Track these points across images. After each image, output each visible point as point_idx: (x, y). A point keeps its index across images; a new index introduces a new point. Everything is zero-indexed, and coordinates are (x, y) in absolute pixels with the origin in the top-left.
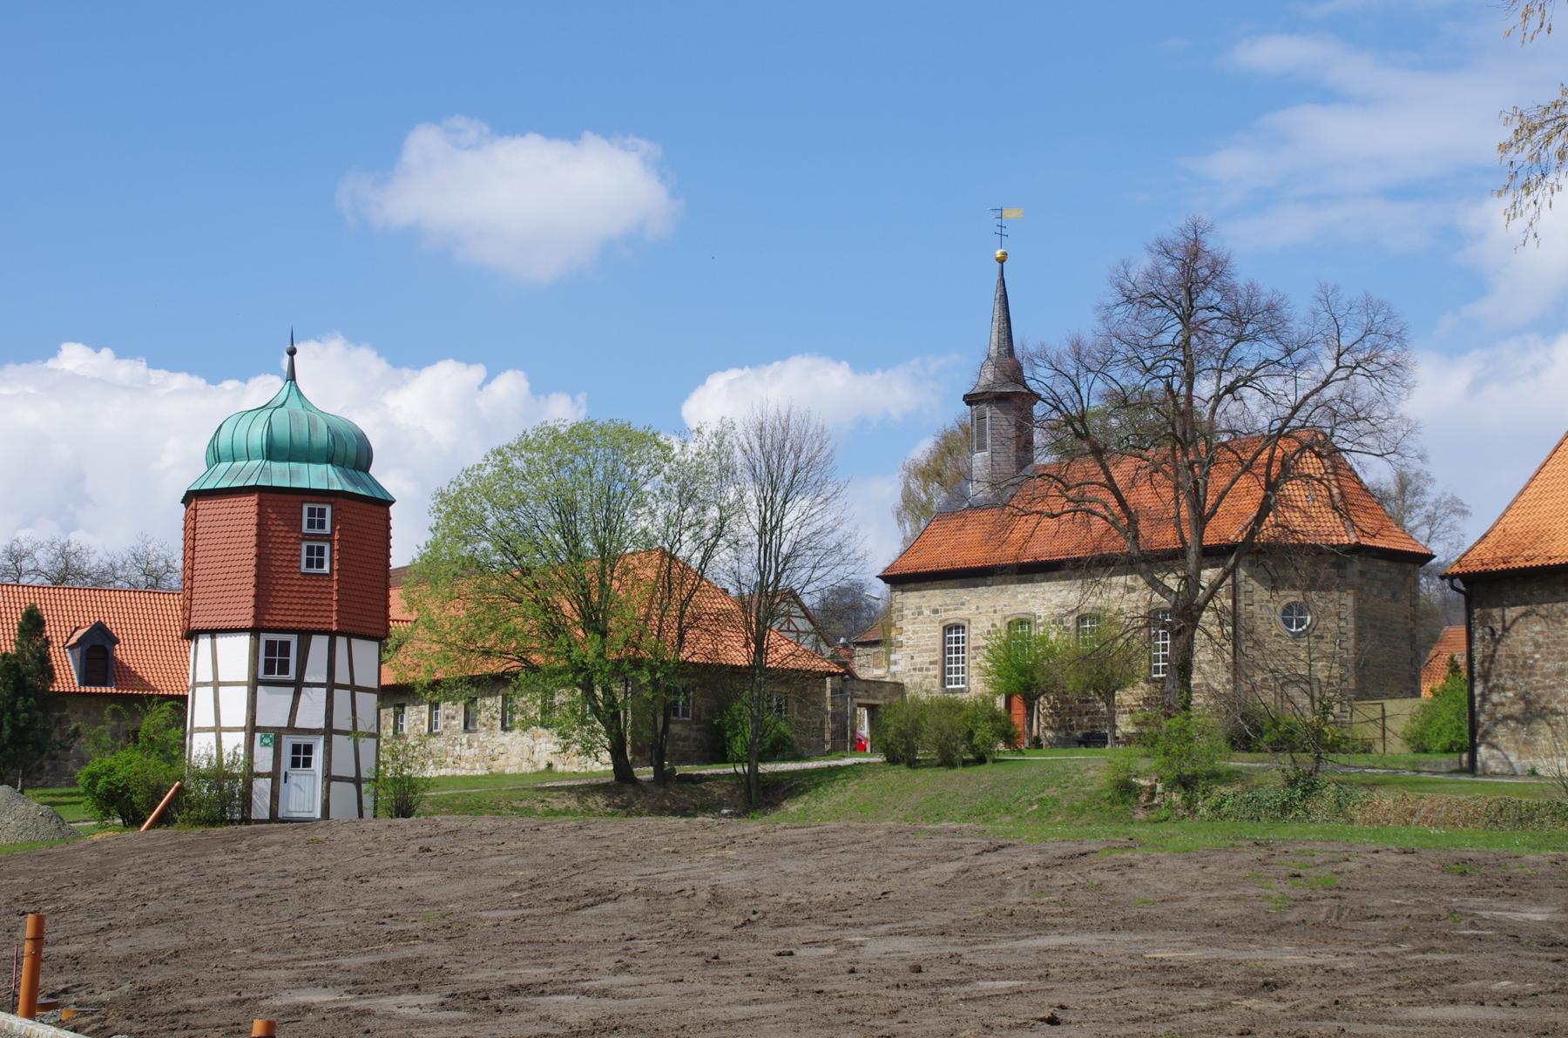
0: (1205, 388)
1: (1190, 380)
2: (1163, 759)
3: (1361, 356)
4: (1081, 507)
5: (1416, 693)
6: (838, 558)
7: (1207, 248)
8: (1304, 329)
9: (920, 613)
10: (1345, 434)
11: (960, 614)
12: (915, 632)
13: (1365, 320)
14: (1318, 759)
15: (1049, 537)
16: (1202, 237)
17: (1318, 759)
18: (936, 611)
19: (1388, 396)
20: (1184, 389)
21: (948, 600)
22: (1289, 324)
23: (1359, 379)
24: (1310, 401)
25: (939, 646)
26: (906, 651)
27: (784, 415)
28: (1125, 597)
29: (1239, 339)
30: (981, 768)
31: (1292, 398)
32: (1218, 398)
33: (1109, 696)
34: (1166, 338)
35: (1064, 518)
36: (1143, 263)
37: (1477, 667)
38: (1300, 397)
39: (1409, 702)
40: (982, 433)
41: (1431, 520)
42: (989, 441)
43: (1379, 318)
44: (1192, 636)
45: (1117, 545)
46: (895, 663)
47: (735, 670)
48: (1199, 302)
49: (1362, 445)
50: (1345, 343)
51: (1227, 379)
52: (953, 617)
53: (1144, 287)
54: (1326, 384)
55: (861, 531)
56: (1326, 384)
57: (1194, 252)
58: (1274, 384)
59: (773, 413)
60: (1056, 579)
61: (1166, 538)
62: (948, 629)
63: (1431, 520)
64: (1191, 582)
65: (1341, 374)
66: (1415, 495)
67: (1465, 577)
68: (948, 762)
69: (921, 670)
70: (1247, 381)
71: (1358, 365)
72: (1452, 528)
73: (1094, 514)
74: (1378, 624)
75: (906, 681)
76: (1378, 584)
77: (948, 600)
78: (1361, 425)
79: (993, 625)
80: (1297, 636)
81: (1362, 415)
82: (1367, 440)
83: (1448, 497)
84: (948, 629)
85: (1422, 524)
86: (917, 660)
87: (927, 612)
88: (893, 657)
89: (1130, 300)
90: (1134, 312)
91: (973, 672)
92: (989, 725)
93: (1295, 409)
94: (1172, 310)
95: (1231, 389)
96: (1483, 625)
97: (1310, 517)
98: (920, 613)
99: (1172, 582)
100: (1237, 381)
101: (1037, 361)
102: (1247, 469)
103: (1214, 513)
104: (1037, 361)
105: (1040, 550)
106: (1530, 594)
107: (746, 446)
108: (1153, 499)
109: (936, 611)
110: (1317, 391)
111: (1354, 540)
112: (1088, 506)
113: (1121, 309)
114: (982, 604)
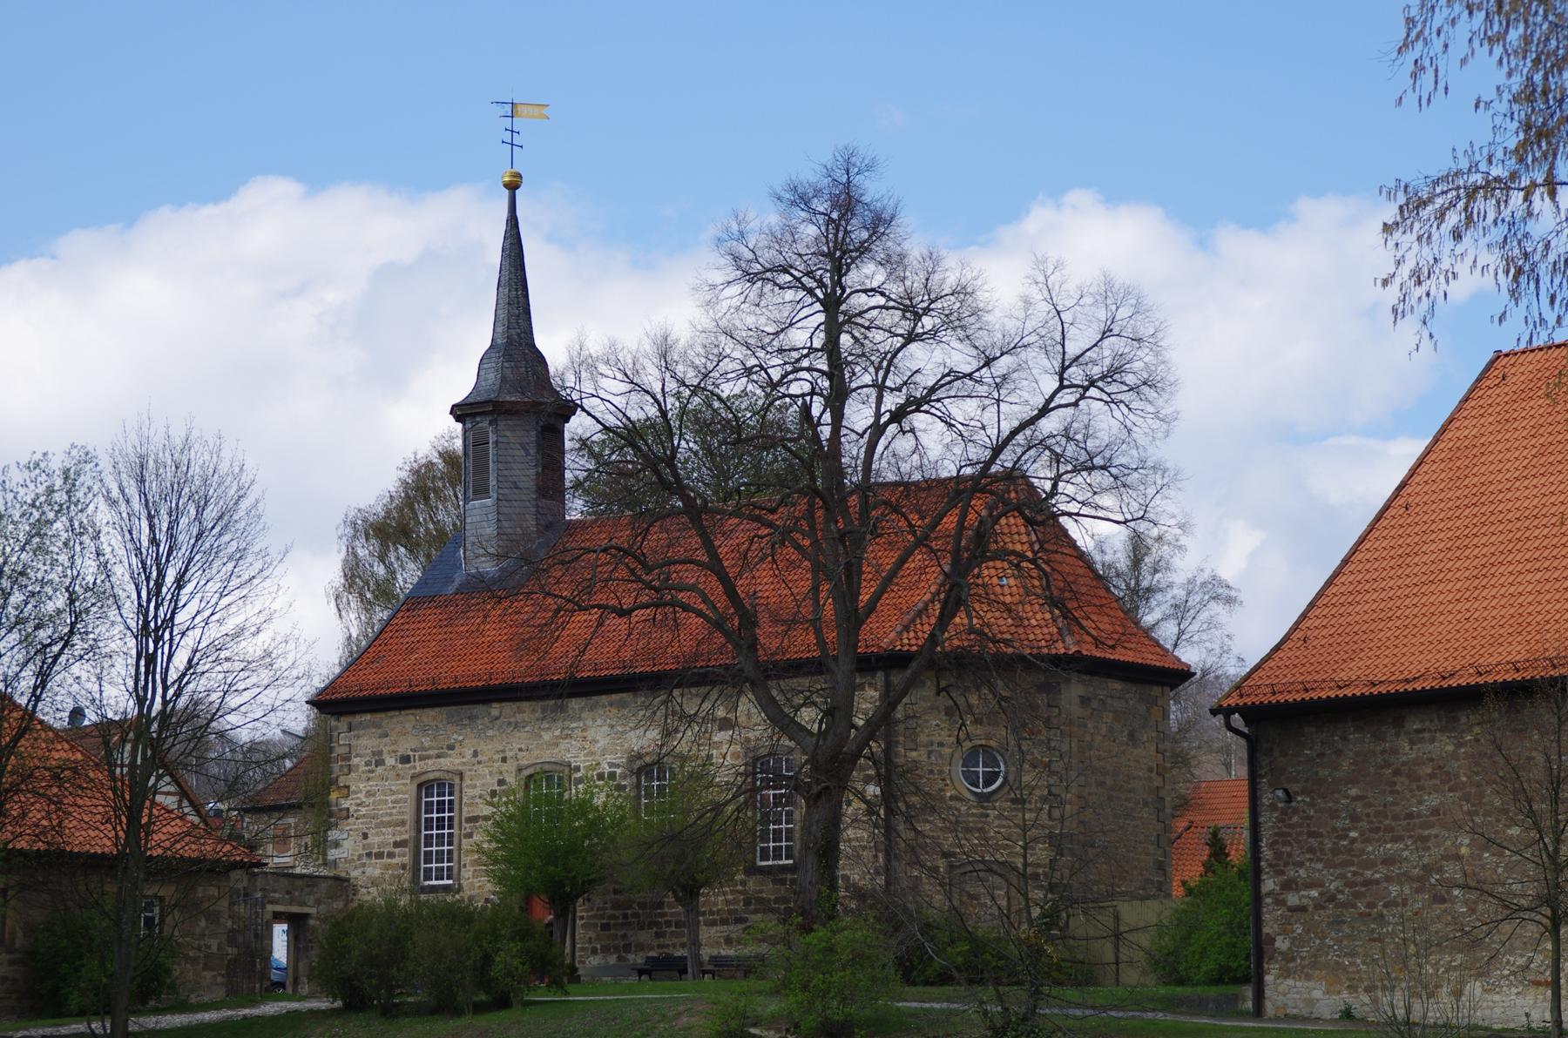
0: (859, 415)
1: (837, 399)
2: (800, 997)
3: (1096, 371)
4: (664, 599)
5: (1162, 890)
6: (265, 676)
7: (866, 199)
8: (1012, 326)
9: (380, 763)
10: (1070, 490)
11: (445, 763)
12: (369, 794)
13: (1102, 315)
14: (1036, 993)
15: (612, 644)
16: (857, 180)
17: (1036, 993)
18: (405, 759)
19: (1137, 433)
20: (827, 417)
21: (427, 742)
22: (988, 318)
23: (1094, 406)
24: (1020, 438)
25: (409, 817)
26: (353, 824)
27: (178, 443)
28: (727, 742)
29: (911, 338)
30: (503, 1014)
31: (993, 432)
32: (877, 430)
33: (689, 893)
34: (799, 337)
35: (638, 615)
36: (765, 218)
37: (1266, 852)
38: (1006, 432)
39: (1154, 905)
40: (481, 467)
41: (1180, 611)
42: (493, 482)
43: (1123, 313)
44: (41, 722)
45: (719, 652)
46: (337, 845)
47: (95, 863)
48: (852, 279)
49: (1097, 507)
50: (1073, 349)
51: (891, 402)
52: (432, 767)
53: (768, 256)
54: (1044, 411)
55: (280, 632)
56: (1044, 411)
57: (846, 202)
58: (963, 410)
59: (158, 440)
60: (622, 705)
61: (802, 644)
62: (425, 787)
63: (1180, 611)
64: (837, 713)
65: (1067, 397)
66: (1156, 571)
67: (1249, 713)
68: (445, 1006)
69: (380, 855)
70: (916, 404)
71: (1092, 383)
72: (1211, 624)
73: (686, 608)
74: (1109, 781)
75: (355, 874)
76: (1108, 717)
77: (427, 742)
78: (1097, 478)
79: (501, 782)
80: (983, 798)
81: (1098, 461)
82: (1107, 500)
83: (1206, 576)
84: (425, 787)
85: (1165, 618)
86: (374, 839)
87: (390, 761)
88: (333, 835)
89: (751, 278)
90: (753, 296)
91: (466, 860)
92: (515, 947)
93: (997, 450)
94: (811, 292)
95: (898, 415)
96: (1274, 785)
97: (1011, 611)
98: (380, 763)
99: (808, 717)
100: (908, 402)
101: (602, 368)
102: (922, 542)
103: (871, 607)
104: (602, 368)
105: (603, 658)
106: (1344, 738)
107: (115, 493)
108: (778, 585)
109: (405, 759)
110: (1032, 421)
111: (1073, 649)
112: (237, 470)
113: (735, 289)
114: (482, 747)
